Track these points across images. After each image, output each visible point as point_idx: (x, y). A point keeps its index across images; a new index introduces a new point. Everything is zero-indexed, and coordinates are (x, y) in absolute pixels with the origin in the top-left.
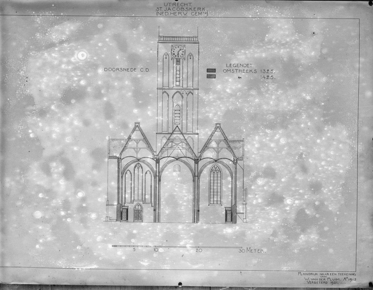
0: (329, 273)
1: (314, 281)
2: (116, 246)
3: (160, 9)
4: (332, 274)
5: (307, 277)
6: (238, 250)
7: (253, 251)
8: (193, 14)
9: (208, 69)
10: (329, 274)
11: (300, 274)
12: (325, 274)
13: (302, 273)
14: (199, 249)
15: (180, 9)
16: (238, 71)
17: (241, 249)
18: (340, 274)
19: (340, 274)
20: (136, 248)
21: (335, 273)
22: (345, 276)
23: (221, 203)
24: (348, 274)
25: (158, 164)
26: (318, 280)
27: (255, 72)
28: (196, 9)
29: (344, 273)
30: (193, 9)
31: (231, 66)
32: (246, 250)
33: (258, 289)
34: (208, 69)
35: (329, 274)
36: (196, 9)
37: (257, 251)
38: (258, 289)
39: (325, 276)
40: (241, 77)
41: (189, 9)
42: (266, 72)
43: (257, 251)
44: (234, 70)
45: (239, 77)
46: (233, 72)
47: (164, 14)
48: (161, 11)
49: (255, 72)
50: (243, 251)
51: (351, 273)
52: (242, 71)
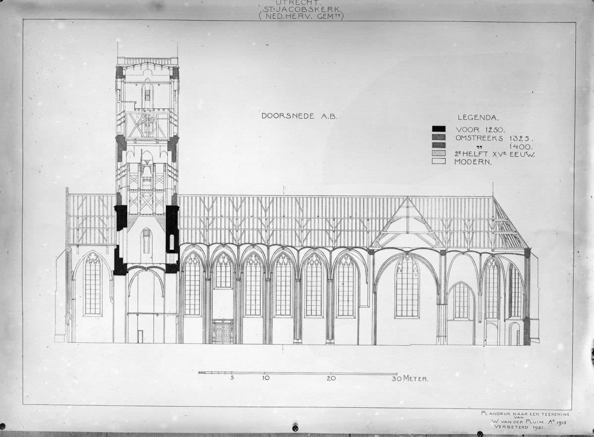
1: (506, 425)
2: (204, 373)
4: (532, 414)
5: (495, 418)
6: (391, 377)
7: (413, 379)
9: (444, 147)
10: (529, 414)
11: (484, 414)
12: (523, 414)
13: (488, 412)
15: (301, 9)
18: (544, 414)
19: (544, 414)
20: (235, 376)
22: (552, 418)
23: (399, 317)
25: (172, 237)
26: (512, 422)
29: (548, 412)
31: (489, 139)
32: (403, 379)
33: (313, 436)
34: (444, 147)
35: (529, 414)
37: (417, 379)
38: (313, 436)
39: (522, 416)
40: (481, 147)
41: (314, 9)
43: (417, 379)
44: (472, 137)
51: (495, 411)
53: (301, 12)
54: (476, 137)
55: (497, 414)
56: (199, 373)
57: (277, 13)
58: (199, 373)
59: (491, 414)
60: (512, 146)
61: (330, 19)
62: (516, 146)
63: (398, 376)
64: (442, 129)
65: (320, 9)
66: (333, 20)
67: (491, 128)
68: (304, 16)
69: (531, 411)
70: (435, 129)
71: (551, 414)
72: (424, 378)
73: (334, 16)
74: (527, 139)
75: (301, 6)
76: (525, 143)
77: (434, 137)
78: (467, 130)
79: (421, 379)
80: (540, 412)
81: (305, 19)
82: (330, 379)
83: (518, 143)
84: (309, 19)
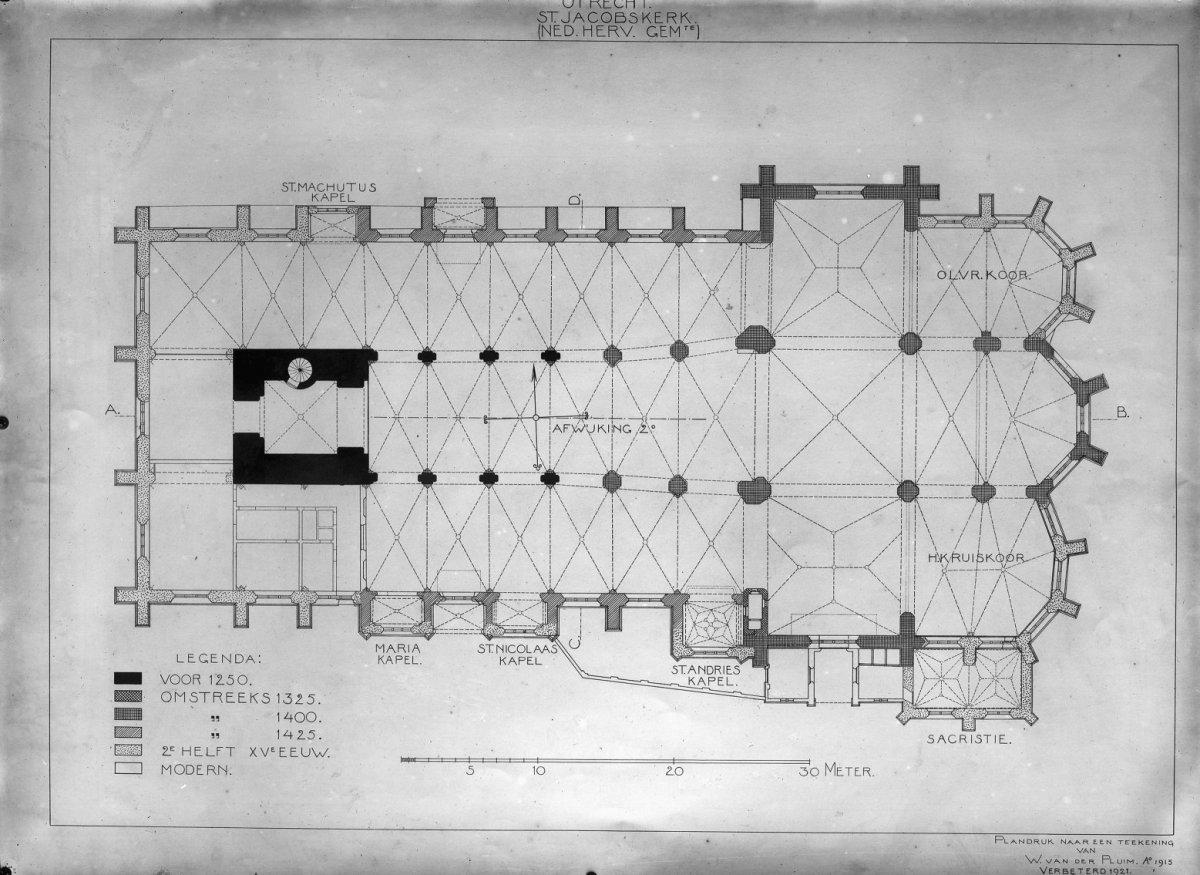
0: (1091, 839)
3: (548, 15)
7: (844, 772)
8: (652, 32)
10: (1098, 842)
14: (674, 767)
16: (209, 697)
17: (808, 767)
21: (1109, 838)
24: (1150, 842)
27: (266, 700)
28: (663, 19)
30: (652, 17)
36: (663, 19)
42: (295, 701)
43: (852, 771)
45: (213, 717)
46: (194, 699)
47: (560, 32)
48: (553, 24)
49: (266, 700)
50: (814, 772)
52: (224, 697)
53: (613, 23)
54: (209, 697)
55: (1029, 842)
56: (403, 760)
57: (563, 25)
58: (403, 760)
59: (1014, 841)
60: (282, 717)
61: (675, 36)
62: (289, 716)
63: (812, 766)
64: (136, 678)
65: (652, 17)
66: (681, 39)
67: (220, 676)
68: (620, 32)
69: (1093, 837)
70: (120, 678)
71: (1150, 842)
72: (867, 770)
73: (682, 29)
74: (311, 701)
75: (613, 11)
76: (304, 709)
77: (119, 696)
78: (181, 679)
79: (860, 772)
80: (1114, 839)
81: (623, 37)
82: (672, 772)
83: (293, 709)
84: (630, 38)
